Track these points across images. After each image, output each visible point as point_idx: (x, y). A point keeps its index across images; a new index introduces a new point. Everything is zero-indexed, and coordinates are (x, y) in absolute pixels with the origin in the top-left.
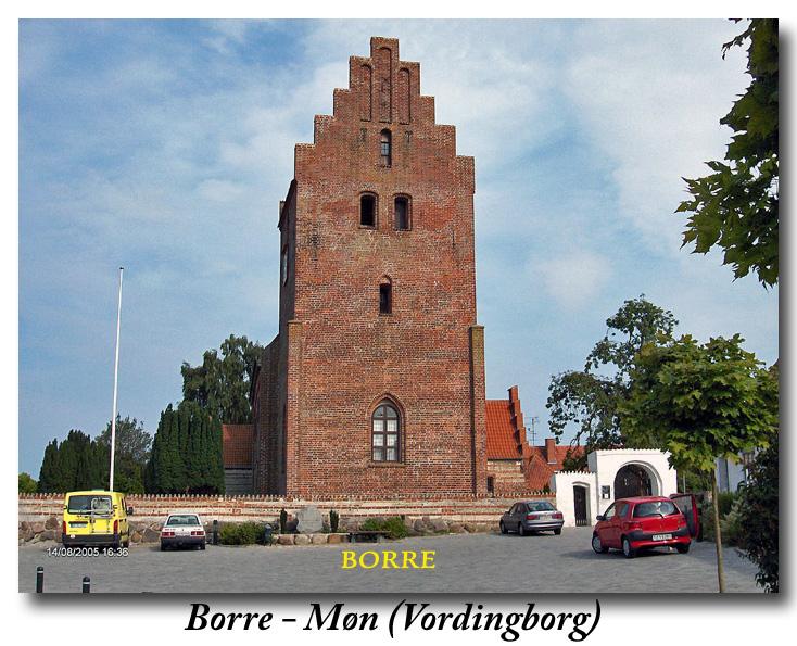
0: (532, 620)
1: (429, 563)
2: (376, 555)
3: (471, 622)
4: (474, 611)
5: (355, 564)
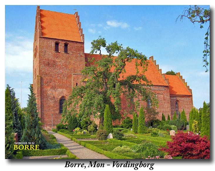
0: (141, 165)
1: (37, 148)
2: (23, 146)
3: (128, 165)
4: (128, 163)
5: (17, 149)
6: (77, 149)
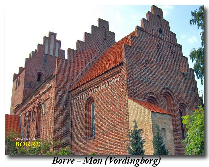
3: (127, 162)
4: (128, 159)
6: (19, 82)
